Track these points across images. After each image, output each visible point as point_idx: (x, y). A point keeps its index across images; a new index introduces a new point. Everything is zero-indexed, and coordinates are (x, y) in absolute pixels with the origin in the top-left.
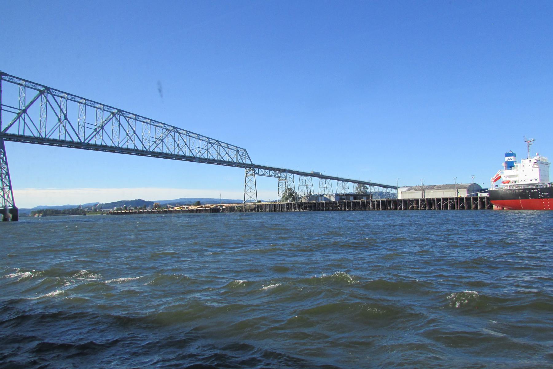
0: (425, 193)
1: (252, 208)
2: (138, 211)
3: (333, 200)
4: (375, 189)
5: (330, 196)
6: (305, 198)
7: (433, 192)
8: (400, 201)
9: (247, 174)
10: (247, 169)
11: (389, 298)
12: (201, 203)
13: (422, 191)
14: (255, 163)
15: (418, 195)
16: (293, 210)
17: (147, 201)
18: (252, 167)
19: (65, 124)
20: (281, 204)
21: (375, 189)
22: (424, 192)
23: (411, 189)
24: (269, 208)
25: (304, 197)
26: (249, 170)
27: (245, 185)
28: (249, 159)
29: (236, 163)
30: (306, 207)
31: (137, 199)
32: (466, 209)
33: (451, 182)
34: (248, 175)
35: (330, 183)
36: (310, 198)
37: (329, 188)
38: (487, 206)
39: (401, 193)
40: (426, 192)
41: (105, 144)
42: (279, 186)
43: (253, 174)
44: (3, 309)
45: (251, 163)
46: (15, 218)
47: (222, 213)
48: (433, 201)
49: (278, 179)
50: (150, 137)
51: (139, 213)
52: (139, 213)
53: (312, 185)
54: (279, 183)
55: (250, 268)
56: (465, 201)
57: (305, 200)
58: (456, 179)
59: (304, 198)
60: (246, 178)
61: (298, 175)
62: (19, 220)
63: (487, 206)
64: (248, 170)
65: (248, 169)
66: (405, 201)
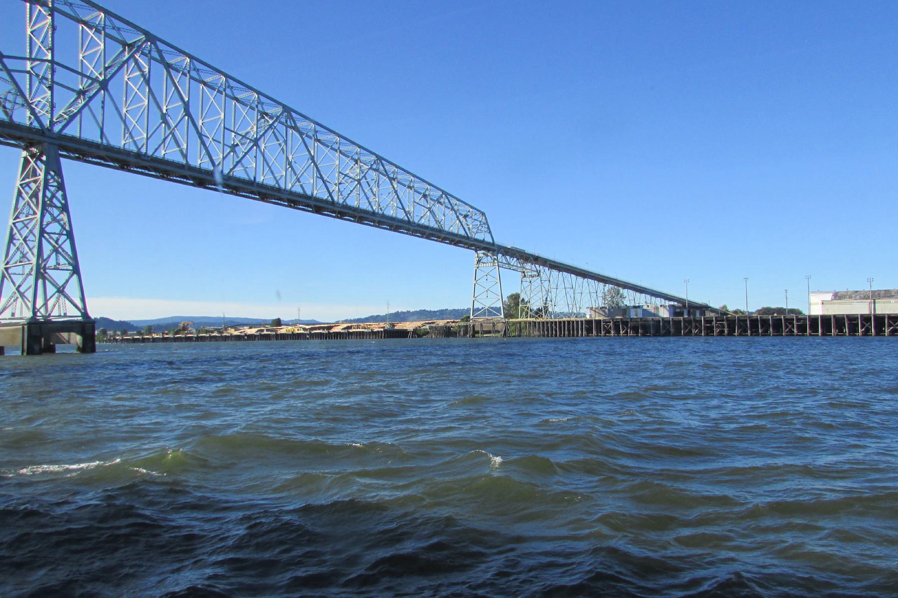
0: (876, 305)
2: (141, 337)
3: (665, 316)
5: (657, 308)
6: (597, 310)
7: (895, 302)
8: (814, 320)
9: (479, 261)
11: (396, 493)
12: (282, 323)
13: (870, 301)
14: (501, 240)
15: (860, 308)
16: (631, 333)
17: (118, 320)
18: (491, 248)
19: (152, 132)
20: (573, 322)
22: (874, 303)
23: (837, 296)
25: (595, 309)
26: (484, 254)
28: (490, 232)
30: (635, 329)
32: (875, 335)
33: (865, 287)
36: (609, 310)
38: (863, 330)
39: (823, 303)
40: (879, 303)
44: (169, 488)
46: (88, 346)
48: (809, 321)
49: (520, 274)
50: (340, 173)
51: (144, 340)
52: (144, 340)
55: (782, 409)
58: (870, 281)
59: (595, 311)
62: (57, 352)
63: (863, 330)
65: (482, 252)
66: (826, 320)
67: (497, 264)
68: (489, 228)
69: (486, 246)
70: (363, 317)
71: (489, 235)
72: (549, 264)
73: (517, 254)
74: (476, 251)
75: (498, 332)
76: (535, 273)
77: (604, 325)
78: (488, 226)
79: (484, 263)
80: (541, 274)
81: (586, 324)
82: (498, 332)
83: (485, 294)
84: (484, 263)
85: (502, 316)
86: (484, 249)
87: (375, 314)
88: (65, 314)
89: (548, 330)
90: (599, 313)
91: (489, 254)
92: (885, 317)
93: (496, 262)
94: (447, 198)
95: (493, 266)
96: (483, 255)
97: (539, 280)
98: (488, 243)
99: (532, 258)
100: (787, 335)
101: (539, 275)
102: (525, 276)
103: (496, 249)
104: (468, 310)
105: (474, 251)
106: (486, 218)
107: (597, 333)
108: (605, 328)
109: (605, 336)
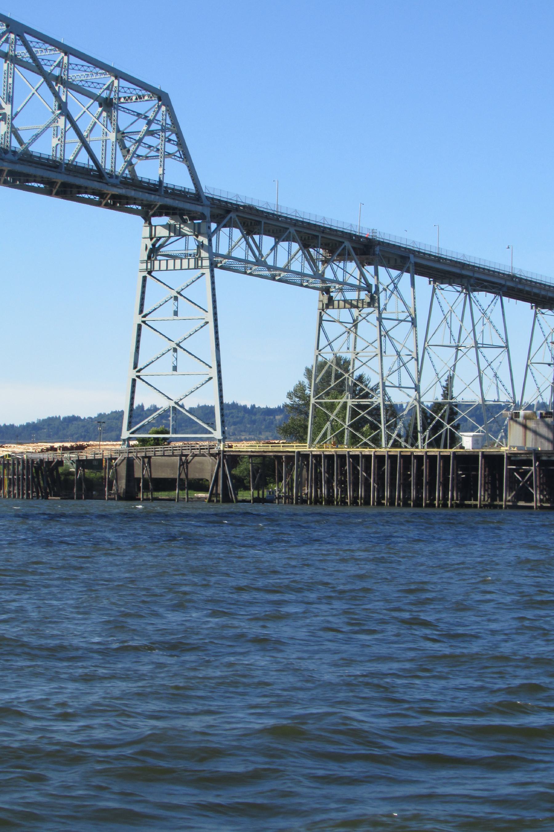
1: (191, 476)
4: (477, 315)
6: (531, 424)
10: (155, 220)
21: (477, 315)
24: (329, 482)
26: (168, 227)
27: (139, 327)
28: (186, 157)
29: (111, 175)
31: (25, 424)
34: (160, 263)
35: (496, 315)
37: (490, 353)
41: (390, 270)
42: (323, 342)
43: (198, 257)
45: (189, 186)
47: (123, 506)
53: (507, 347)
54: (320, 325)
56: (347, 467)
57: (530, 435)
59: (525, 427)
60: (145, 279)
61: (528, 305)
64: (162, 232)
65: (165, 220)
67: (206, 263)
68: (181, 143)
69: (169, 201)
70: (19, 421)
71: (183, 167)
72: (416, 264)
73: (292, 230)
74: (147, 219)
75: (199, 485)
76: (364, 295)
77: (510, 471)
78: (179, 135)
79: (174, 257)
80: (382, 296)
81: (458, 466)
82: (199, 485)
83: (169, 359)
84: (174, 257)
85: (218, 434)
86: (163, 211)
87: (63, 413)
88: (498, 400)
89: (406, 487)
90: (535, 433)
91: (186, 230)
92: (504, 455)
93: (204, 254)
94: (26, 44)
95: (196, 267)
96: (165, 233)
97: (373, 318)
98: (180, 194)
99: (347, 244)
100: (541, 507)
101: (373, 301)
102: (331, 302)
103: (207, 212)
104: (118, 415)
105: (139, 220)
106: (170, 111)
107: (493, 497)
108: (512, 481)
109: (515, 507)
